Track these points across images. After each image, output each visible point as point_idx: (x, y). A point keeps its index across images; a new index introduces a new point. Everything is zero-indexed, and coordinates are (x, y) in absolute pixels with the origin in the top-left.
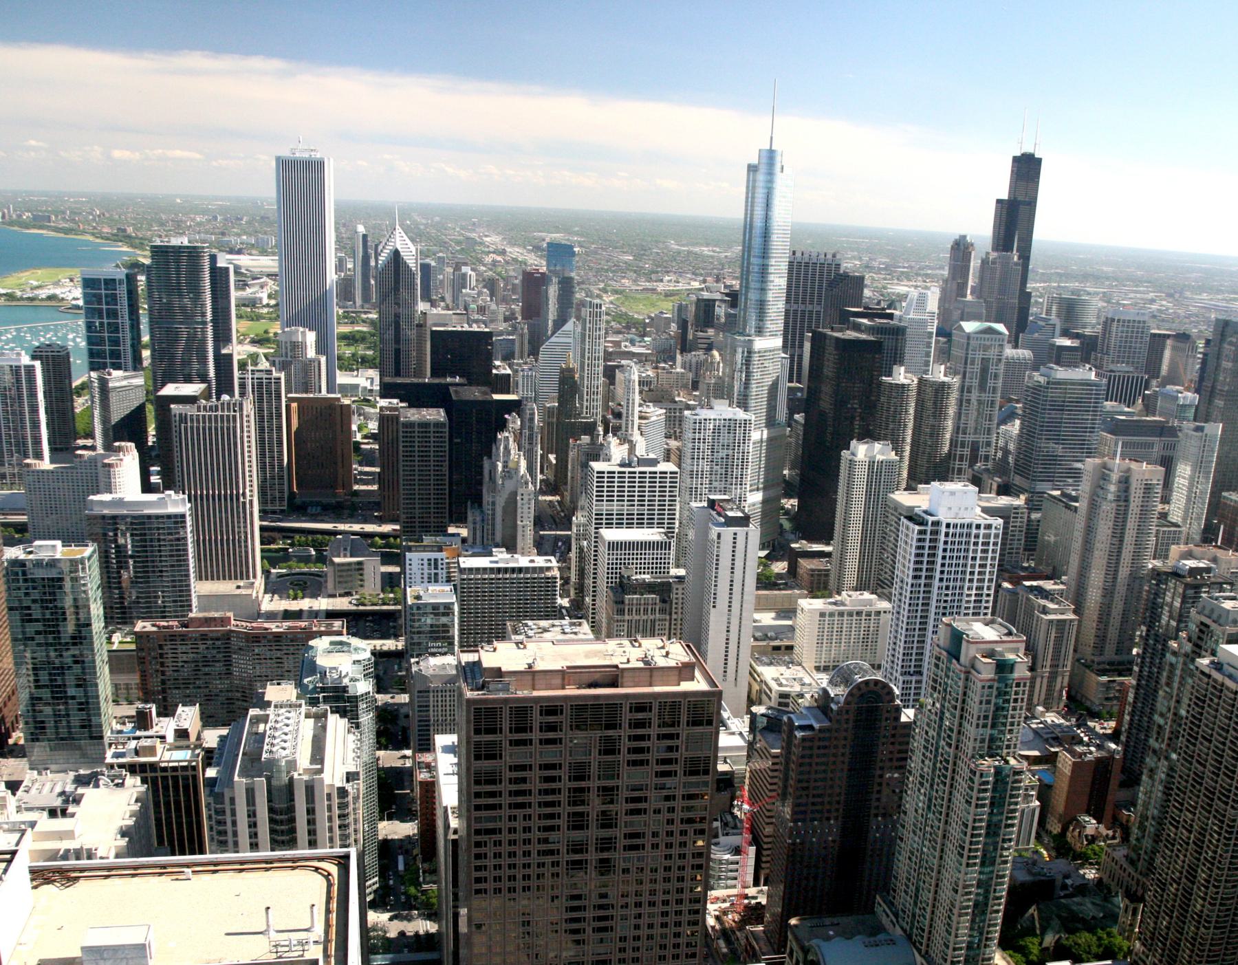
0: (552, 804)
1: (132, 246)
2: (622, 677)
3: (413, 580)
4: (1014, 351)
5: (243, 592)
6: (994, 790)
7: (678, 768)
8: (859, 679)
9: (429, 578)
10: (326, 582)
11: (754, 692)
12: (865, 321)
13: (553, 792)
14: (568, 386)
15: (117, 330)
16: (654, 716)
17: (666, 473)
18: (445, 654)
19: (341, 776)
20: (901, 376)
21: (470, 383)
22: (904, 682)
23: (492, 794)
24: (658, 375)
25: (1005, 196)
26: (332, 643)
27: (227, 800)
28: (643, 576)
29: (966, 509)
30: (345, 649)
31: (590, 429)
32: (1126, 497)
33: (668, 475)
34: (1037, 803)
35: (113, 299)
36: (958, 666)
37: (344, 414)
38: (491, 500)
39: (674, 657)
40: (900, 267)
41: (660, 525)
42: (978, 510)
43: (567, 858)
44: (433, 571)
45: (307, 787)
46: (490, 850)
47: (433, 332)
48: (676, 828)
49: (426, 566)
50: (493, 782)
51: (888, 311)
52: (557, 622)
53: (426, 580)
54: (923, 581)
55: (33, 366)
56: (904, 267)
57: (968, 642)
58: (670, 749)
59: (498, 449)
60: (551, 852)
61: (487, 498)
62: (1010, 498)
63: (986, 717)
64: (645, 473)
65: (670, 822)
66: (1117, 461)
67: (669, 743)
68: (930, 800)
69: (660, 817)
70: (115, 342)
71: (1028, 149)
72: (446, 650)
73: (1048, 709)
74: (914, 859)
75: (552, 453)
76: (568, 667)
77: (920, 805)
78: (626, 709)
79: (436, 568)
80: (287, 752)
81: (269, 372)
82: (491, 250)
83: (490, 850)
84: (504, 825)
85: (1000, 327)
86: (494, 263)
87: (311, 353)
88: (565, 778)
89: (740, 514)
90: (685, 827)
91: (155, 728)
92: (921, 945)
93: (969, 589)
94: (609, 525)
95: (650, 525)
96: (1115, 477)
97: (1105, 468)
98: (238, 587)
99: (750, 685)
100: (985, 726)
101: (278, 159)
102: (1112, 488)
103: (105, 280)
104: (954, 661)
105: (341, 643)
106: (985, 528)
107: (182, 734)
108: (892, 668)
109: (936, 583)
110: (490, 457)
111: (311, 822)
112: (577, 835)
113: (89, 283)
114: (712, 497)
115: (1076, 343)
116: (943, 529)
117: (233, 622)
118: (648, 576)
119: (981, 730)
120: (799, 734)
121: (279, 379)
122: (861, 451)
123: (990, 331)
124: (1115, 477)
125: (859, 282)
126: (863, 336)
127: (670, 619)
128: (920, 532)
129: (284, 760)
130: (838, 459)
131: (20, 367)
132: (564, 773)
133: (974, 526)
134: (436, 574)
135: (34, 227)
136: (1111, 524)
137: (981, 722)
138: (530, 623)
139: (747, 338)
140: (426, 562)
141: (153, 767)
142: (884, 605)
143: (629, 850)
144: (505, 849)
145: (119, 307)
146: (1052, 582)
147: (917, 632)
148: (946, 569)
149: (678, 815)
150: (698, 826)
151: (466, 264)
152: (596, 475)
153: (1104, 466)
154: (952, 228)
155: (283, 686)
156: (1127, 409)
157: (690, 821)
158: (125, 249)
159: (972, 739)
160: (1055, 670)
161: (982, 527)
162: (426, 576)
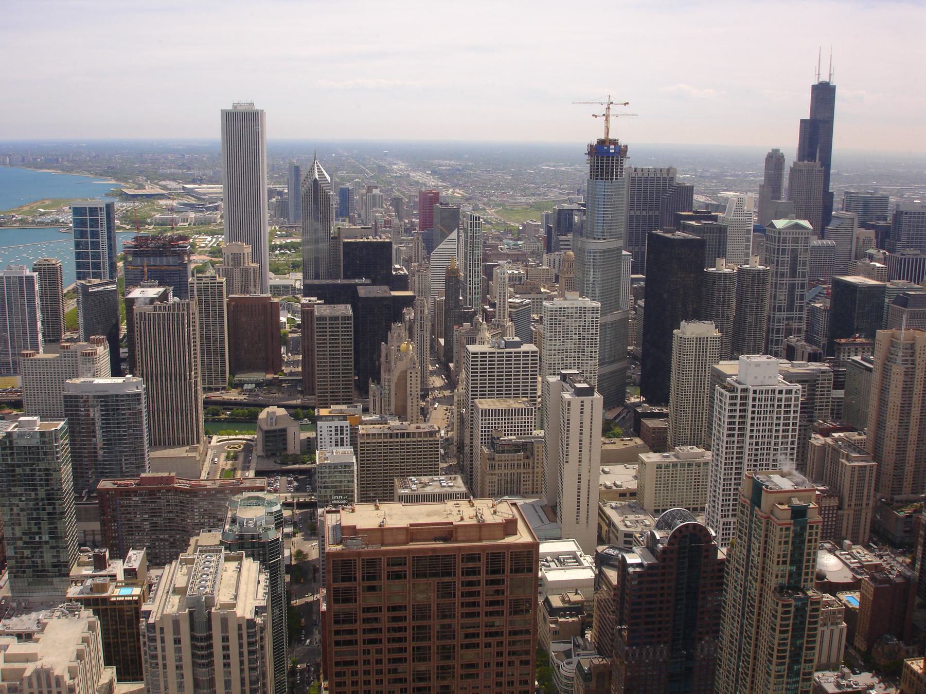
0: (400, 640)
1: (118, 180)
2: (456, 533)
3: (323, 444)
4: (820, 242)
5: (190, 455)
6: (795, 618)
7: (505, 608)
9: (336, 442)
10: (256, 445)
11: (604, 533)
12: (693, 223)
13: (400, 629)
14: (452, 280)
16: (482, 565)
19: (251, 609)
20: (724, 267)
21: (374, 283)
22: (724, 524)
23: (350, 632)
24: (527, 272)
25: (808, 117)
27: (158, 630)
28: (510, 437)
29: (770, 377)
30: (260, 503)
31: (470, 317)
33: (530, 354)
34: (844, 624)
35: (94, 223)
36: (759, 512)
37: (272, 311)
38: (387, 377)
39: (500, 514)
40: (727, 176)
41: (525, 394)
42: (780, 378)
43: (413, 685)
44: (339, 436)
45: (222, 619)
46: (348, 679)
47: (344, 243)
49: (333, 433)
50: (351, 622)
51: (713, 214)
52: (436, 478)
53: (334, 443)
54: (736, 439)
55: (33, 277)
57: (767, 492)
58: (498, 592)
61: (384, 375)
62: (818, 364)
63: (785, 555)
64: (511, 353)
65: (500, 654)
66: (903, 331)
67: (496, 587)
68: (742, 626)
69: (491, 650)
70: (96, 256)
71: (824, 78)
72: (346, 502)
73: (855, 542)
74: (731, 677)
75: (441, 337)
76: (411, 525)
77: (735, 630)
78: (458, 560)
79: (342, 434)
80: (208, 590)
81: (214, 278)
83: (348, 679)
84: (361, 658)
85: (805, 223)
88: (409, 617)
89: (585, 385)
91: (109, 569)
93: (775, 444)
94: (483, 396)
95: (516, 396)
97: (893, 337)
99: (600, 527)
100: (784, 563)
101: (222, 111)
103: (90, 208)
104: (756, 508)
105: (258, 498)
106: (786, 393)
107: (130, 573)
108: (714, 512)
109: (748, 440)
110: (386, 343)
112: (422, 667)
113: (77, 211)
114: (563, 372)
116: (751, 395)
118: (514, 437)
119: (782, 567)
122: (690, 330)
123: (797, 226)
125: (689, 191)
126: (690, 236)
127: (533, 473)
128: (732, 398)
129: (204, 597)
130: (671, 336)
131: (22, 277)
132: (409, 613)
133: (784, 392)
134: (342, 439)
135: (46, 168)
137: (781, 559)
138: (414, 479)
140: (333, 429)
141: (105, 600)
142: (708, 455)
144: (361, 678)
145: (100, 229)
146: (856, 433)
147: (733, 482)
148: (755, 428)
149: (506, 649)
150: (524, 658)
151: (376, 188)
152: (471, 356)
153: (893, 336)
154: (765, 145)
155: (213, 532)
158: (113, 182)
159: (774, 575)
160: (859, 508)
161: (784, 392)
162: (333, 441)
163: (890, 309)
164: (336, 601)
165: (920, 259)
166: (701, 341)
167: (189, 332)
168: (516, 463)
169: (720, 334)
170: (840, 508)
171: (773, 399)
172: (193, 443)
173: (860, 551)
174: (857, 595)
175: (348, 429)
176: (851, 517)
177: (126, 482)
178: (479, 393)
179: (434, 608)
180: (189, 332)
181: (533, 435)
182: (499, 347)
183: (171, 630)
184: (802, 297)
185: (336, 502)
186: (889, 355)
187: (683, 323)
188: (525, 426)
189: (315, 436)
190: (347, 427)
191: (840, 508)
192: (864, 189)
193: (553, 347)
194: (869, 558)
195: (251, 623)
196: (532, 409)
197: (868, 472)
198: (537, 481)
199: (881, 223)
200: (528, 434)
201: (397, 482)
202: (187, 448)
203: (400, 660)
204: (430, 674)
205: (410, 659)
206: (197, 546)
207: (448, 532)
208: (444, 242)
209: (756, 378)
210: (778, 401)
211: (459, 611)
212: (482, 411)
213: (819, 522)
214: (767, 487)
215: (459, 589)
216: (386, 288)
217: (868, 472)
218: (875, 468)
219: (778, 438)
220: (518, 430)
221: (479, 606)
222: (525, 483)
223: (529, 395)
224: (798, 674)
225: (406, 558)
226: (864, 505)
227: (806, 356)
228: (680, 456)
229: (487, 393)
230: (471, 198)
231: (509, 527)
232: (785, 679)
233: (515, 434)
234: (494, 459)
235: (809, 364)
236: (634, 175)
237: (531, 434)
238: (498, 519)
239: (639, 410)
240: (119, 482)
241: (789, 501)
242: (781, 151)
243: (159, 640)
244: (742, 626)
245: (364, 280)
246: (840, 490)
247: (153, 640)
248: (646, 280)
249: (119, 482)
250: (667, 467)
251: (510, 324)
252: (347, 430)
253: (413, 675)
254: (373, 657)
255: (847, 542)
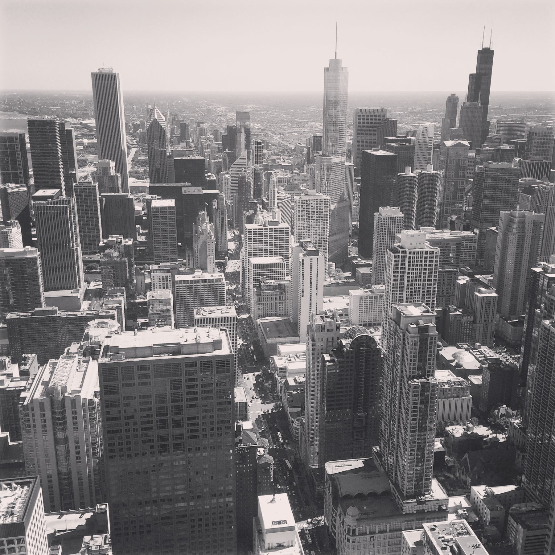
3: (155, 287)
5: (74, 295)
8: (358, 335)
12: (393, 144)
15: (16, 170)
17: (283, 228)
18: (164, 325)
26: (98, 323)
28: (271, 281)
29: (420, 244)
32: (523, 230)
34: (471, 396)
36: (399, 329)
41: (281, 255)
42: (427, 244)
48: (216, 426)
53: (162, 287)
56: (430, 112)
57: (403, 316)
59: (199, 219)
60: (150, 441)
64: (273, 229)
68: (392, 399)
73: (483, 344)
76: (154, 345)
80: (63, 382)
81: (90, 183)
82: (220, 114)
85: (466, 143)
86: (221, 121)
87: (113, 172)
90: (220, 425)
92: (392, 478)
94: (255, 256)
95: (276, 255)
96: (516, 220)
98: (71, 293)
102: (515, 226)
105: (104, 323)
106: (430, 253)
109: (406, 283)
110: (195, 224)
111: (75, 418)
112: (162, 432)
114: (301, 241)
115: (512, 147)
117: (58, 312)
118: (273, 281)
120: (328, 364)
121: (95, 186)
124: (516, 220)
125: (395, 122)
133: (424, 253)
136: (515, 245)
139: (328, 158)
143: (191, 438)
146: (490, 275)
152: (247, 231)
153: (511, 215)
156: (538, 181)
157: (222, 422)
161: (429, 253)
163: (520, 196)
164: (106, 393)
165: (543, 163)
166: (391, 220)
167: (71, 217)
168: (274, 297)
169: (403, 215)
170: (474, 322)
171: (421, 257)
172: (76, 287)
173: (486, 350)
174: (480, 377)
175: (171, 277)
176: (482, 328)
177: (25, 314)
178: (258, 254)
179: (169, 395)
180: (71, 217)
181: (286, 279)
182: (264, 226)
183: (39, 409)
184: (462, 190)
185: (158, 323)
186: (508, 227)
187: (381, 208)
188: (278, 274)
189: (150, 282)
190: (170, 276)
191: (474, 322)
192: (511, 118)
193: (300, 224)
194: (490, 354)
195: (91, 402)
196: (284, 263)
197: (492, 301)
198: (287, 307)
199: (520, 141)
200: (282, 279)
201: (195, 310)
202: (73, 291)
203: (149, 429)
204: (168, 436)
205: (155, 428)
206: (68, 353)
207: (177, 349)
208: (238, 159)
209: (411, 244)
210: (425, 258)
211: (185, 397)
212: (254, 265)
213: (436, 336)
214: (404, 314)
215: (184, 384)
216: (200, 188)
217: (492, 301)
218: (497, 298)
219: (425, 281)
220: (278, 277)
221: (197, 394)
222: (280, 309)
223: (284, 255)
224: (425, 430)
225: (149, 365)
226: (490, 321)
227: (462, 227)
228: (375, 291)
229: (263, 253)
230: (264, 130)
231: (217, 344)
232: (417, 433)
233: (274, 279)
234: (261, 295)
235: (462, 232)
236: (360, 114)
237: (284, 279)
238: (210, 340)
239: (354, 262)
240: (21, 314)
241: (417, 323)
242: (456, 96)
243: (31, 415)
244: (392, 399)
245: (187, 184)
246: (474, 311)
247: (27, 415)
248: (31, 231)
249: (21, 314)
250: (366, 298)
251: (278, 210)
252: (170, 279)
253: (158, 437)
254: (131, 427)
255: (478, 344)
